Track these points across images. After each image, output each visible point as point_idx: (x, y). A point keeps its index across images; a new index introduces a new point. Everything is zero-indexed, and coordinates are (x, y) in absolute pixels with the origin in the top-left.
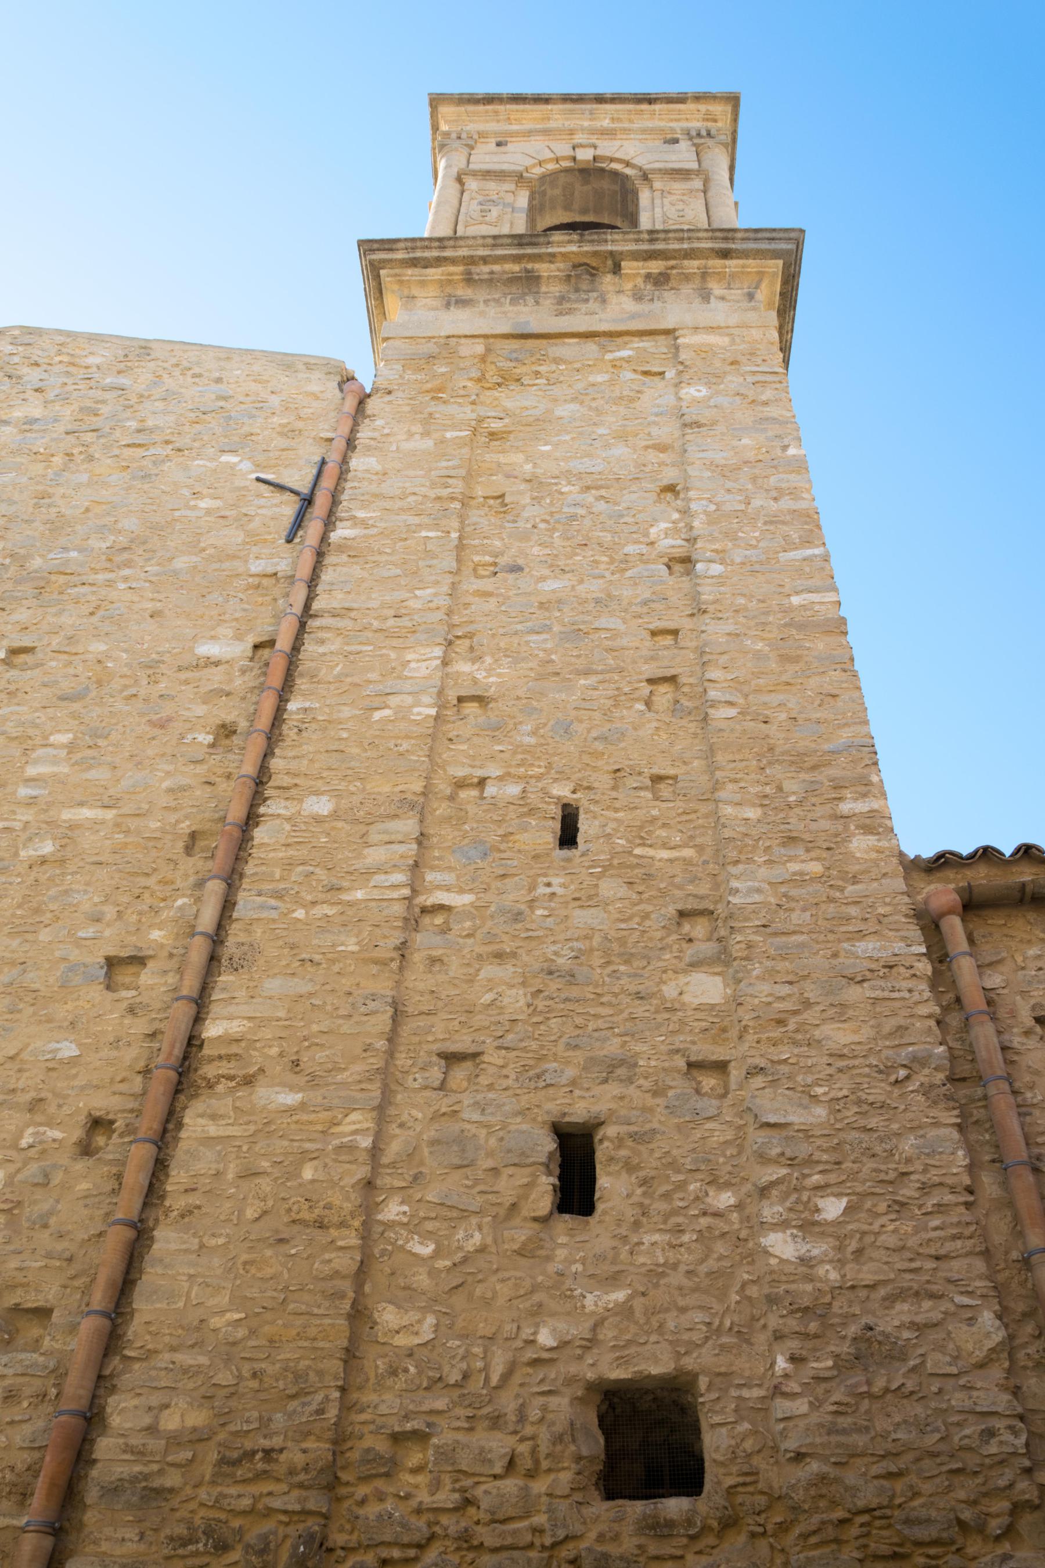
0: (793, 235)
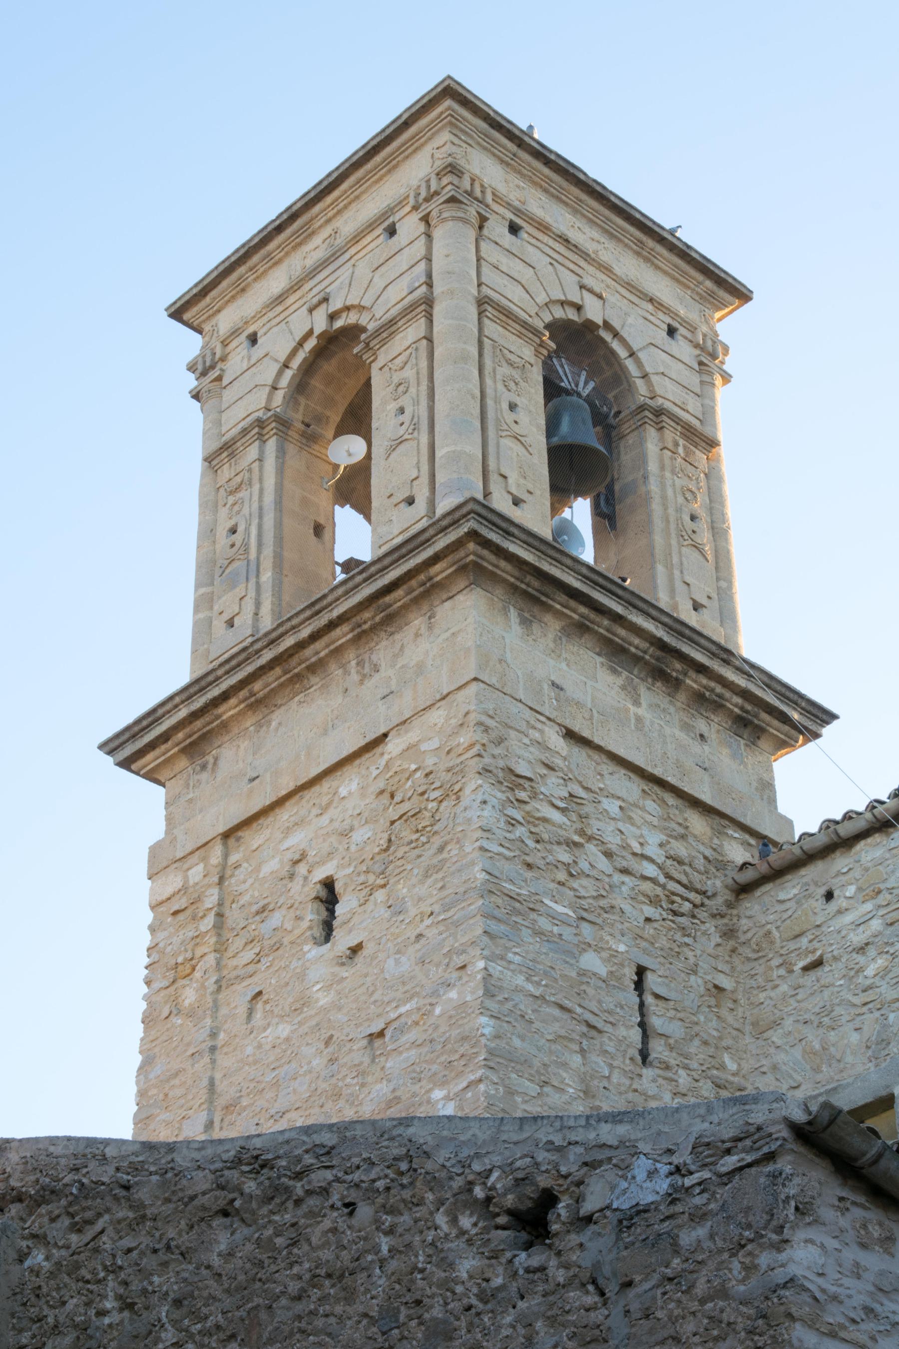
0: (464, 510)
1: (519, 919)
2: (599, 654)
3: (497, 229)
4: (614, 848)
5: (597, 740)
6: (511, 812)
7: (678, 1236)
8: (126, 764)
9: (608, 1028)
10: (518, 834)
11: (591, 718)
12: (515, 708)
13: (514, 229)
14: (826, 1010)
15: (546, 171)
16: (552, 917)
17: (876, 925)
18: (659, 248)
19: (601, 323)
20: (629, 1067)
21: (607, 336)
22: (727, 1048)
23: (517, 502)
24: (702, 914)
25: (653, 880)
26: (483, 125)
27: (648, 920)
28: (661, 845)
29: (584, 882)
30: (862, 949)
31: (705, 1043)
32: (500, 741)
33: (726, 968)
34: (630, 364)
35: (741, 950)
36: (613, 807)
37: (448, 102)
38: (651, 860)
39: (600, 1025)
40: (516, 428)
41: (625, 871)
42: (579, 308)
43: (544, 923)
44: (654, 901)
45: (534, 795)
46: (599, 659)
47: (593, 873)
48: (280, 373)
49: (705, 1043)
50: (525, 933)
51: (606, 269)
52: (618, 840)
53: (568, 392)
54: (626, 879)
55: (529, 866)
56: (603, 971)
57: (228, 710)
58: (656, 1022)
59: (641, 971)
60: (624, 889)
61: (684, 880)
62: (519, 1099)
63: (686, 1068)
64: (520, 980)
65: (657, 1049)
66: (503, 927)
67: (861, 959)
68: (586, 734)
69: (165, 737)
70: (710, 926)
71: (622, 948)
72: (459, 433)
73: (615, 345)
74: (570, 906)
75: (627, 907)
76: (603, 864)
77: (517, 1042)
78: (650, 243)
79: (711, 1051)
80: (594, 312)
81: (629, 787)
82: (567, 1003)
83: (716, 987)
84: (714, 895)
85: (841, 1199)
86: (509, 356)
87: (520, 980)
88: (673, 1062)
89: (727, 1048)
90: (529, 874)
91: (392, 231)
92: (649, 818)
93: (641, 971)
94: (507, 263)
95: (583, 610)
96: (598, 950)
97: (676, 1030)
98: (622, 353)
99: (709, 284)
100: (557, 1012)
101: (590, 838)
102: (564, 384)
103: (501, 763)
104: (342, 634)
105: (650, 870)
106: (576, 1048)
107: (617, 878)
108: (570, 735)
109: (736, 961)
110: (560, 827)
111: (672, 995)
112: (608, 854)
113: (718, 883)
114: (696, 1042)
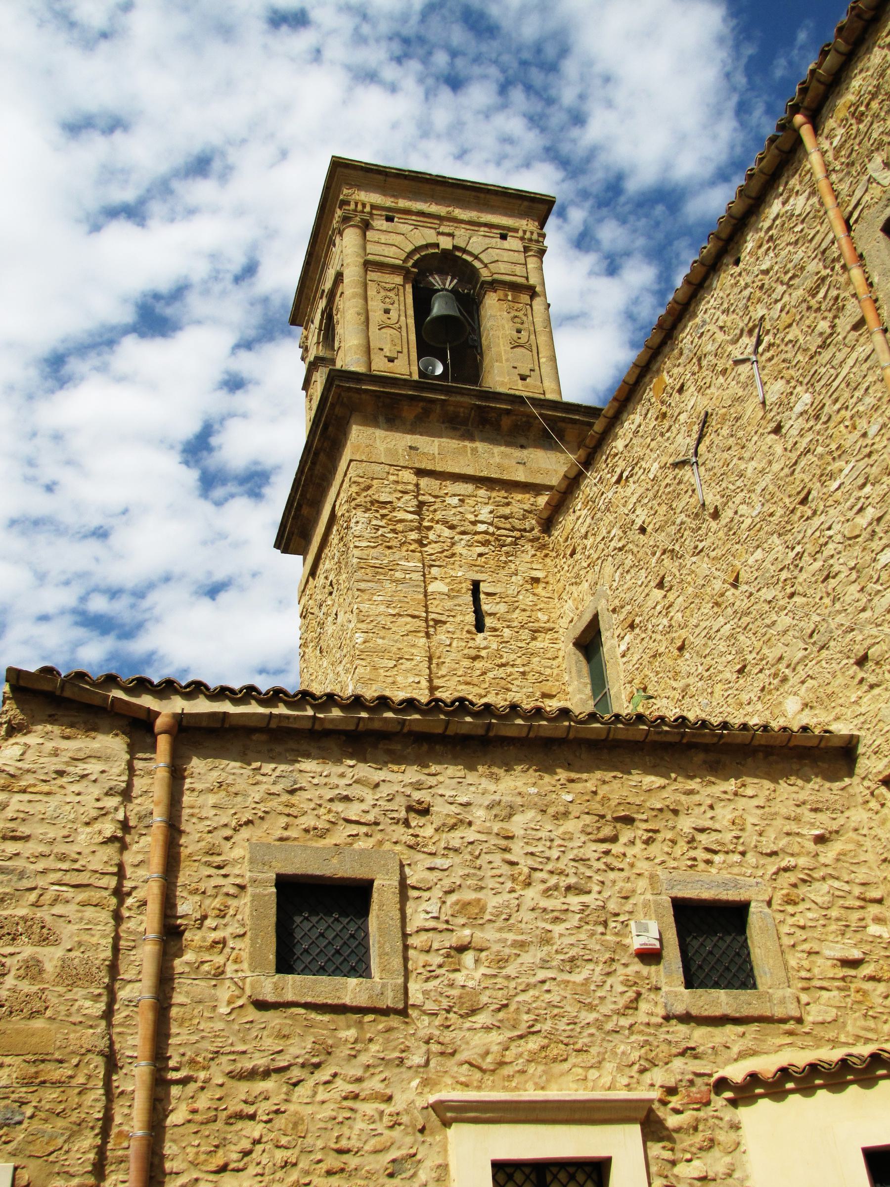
1: (382, 577)
2: (443, 423)
3: (379, 223)
4: (455, 523)
5: (438, 469)
6: (374, 522)
7: (617, 716)
8: (285, 551)
9: (451, 619)
10: (380, 533)
11: (434, 459)
12: (377, 468)
13: (390, 219)
14: (577, 576)
15: (406, 182)
16: (405, 571)
17: (589, 520)
18: (488, 196)
19: (451, 247)
20: (465, 635)
21: (458, 254)
22: (540, 610)
23: (391, 360)
24: (521, 542)
25: (486, 533)
26: (361, 173)
27: (480, 555)
28: (491, 512)
29: (433, 545)
30: (586, 537)
31: (524, 610)
32: (368, 488)
33: (539, 566)
34: (477, 264)
35: (551, 554)
36: (455, 501)
37: (339, 169)
38: (483, 522)
39: (444, 618)
40: (389, 322)
41: (463, 533)
42: (437, 245)
43: (399, 575)
44: (485, 543)
45: (394, 509)
46: (443, 426)
47: (441, 539)
48: (319, 334)
49: (524, 610)
50: (387, 584)
51: (455, 220)
52: (458, 517)
53: (438, 291)
54: (464, 537)
55: (389, 548)
56: (445, 589)
57: (305, 511)
58: (485, 607)
59: (476, 584)
60: (463, 542)
61: (508, 526)
62: (381, 671)
63: (508, 627)
64: (382, 608)
65: (489, 622)
66: (370, 584)
67: (585, 541)
68: (430, 467)
69: (291, 533)
70: (528, 547)
71: (460, 574)
72: (379, 336)
73: (465, 257)
74: (419, 561)
75: (464, 552)
76: (447, 532)
77: (380, 641)
78: (482, 195)
79: (528, 613)
80: (446, 243)
81: (466, 488)
82: (416, 613)
83: (532, 578)
84: (532, 529)
85: (50, 716)
86: (387, 286)
87: (382, 608)
88: (499, 626)
89: (540, 610)
90: (388, 552)
91: (504, 237)
92: (480, 500)
93: (476, 586)
94: (383, 238)
95: (421, 404)
96: (442, 579)
97: (502, 608)
98: (469, 259)
99: (526, 203)
100: (409, 619)
101: (437, 522)
102: (437, 287)
103: (368, 499)
104: (322, 457)
105: (481, 528)
106: (423, 634)
107: (457, 537)
108: (420, 473)
109: (548, 560)
110: (411, 521)
111: (498, 590)
112: (452, 527)
113: (534, 522)
114: (518, 611)
